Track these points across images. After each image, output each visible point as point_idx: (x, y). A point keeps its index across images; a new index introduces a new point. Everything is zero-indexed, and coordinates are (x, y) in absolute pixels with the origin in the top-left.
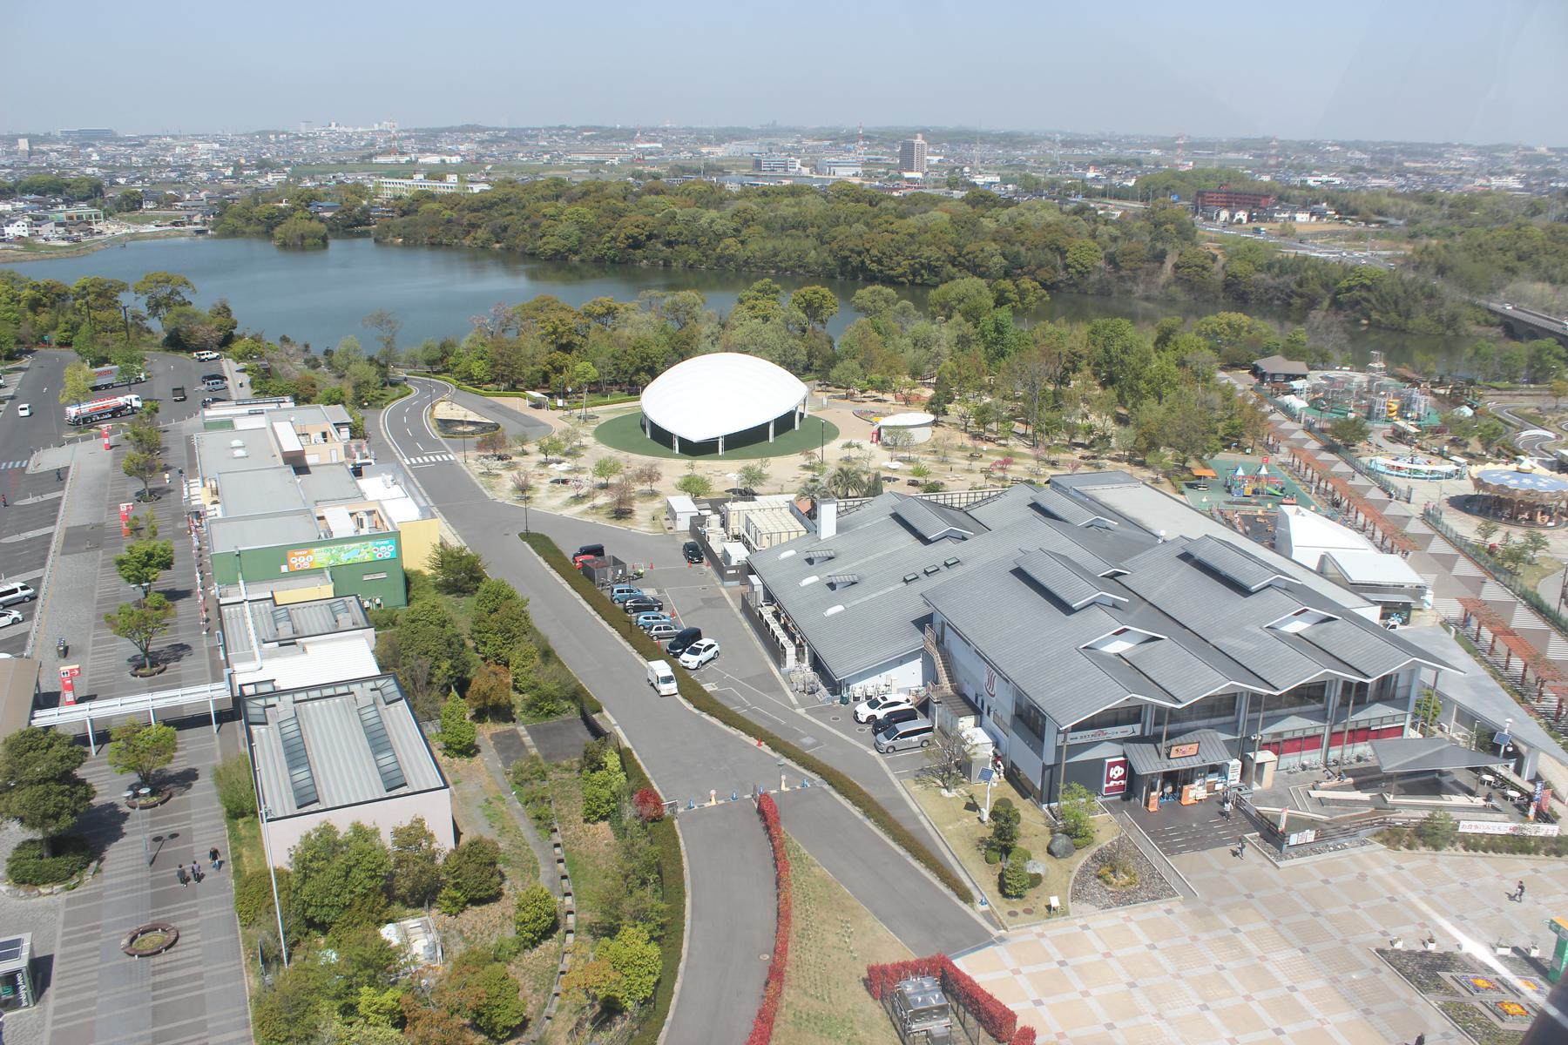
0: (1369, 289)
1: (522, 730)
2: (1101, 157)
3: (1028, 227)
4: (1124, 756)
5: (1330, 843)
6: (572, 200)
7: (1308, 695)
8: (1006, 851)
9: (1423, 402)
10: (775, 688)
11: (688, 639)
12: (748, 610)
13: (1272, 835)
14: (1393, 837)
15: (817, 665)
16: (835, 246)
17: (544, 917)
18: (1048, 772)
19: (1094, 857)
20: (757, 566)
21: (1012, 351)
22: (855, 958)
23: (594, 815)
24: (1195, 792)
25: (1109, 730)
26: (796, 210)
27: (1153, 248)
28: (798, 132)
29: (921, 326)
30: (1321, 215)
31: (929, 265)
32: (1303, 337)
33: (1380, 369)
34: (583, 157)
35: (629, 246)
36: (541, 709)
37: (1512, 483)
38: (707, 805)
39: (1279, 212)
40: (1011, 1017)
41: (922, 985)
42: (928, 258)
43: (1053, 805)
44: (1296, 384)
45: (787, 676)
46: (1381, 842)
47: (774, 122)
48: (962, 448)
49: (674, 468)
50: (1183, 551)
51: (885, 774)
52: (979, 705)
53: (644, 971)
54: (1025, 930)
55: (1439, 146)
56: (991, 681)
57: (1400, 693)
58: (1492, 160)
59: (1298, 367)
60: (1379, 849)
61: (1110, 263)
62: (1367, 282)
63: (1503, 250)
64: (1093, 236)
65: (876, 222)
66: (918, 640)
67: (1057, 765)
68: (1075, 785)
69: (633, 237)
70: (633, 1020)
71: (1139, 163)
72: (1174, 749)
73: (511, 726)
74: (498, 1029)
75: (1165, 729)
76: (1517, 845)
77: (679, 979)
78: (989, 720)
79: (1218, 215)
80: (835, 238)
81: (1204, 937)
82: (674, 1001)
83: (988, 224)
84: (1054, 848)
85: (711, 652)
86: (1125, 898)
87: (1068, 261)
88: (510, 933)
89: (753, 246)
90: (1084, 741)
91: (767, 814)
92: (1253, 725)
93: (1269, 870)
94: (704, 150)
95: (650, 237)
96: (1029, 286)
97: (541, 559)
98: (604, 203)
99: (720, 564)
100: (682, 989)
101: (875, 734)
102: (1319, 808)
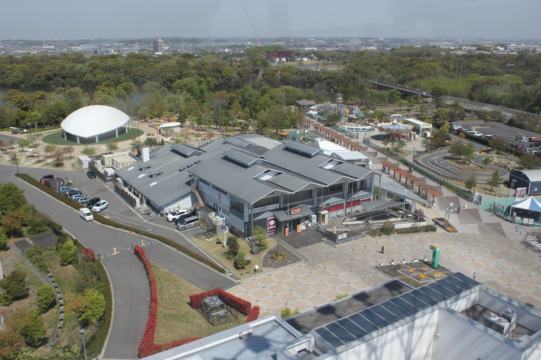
0: (332, 78)
1: (28, 239)
2: (229, 45)
3: (207, 64)
4: (274, 216)
5: (352, 238)
6: (18, 63)
7: (336, 189)
8: (235, 254)
9: (357, 109)
10: (134, 215)
11: (95, 202)
12: (118, 190)
13: (332, 237)
14: (373, 233)
15: (149, 203)
16: (132, 75)
17: (50, 297)
18: (246, 225)
19: (268, 253)
20: (119, 174)
21: (207, 100)
22: (183, 296)
23: (65, 263)
24: (301, 227)
25: (267, 207)
26: (115, 63)
27: (254, 69)
28: (111, 41)
29: (171, 96)
30: (312, 58)
31: (170, 80)
32: (312, 93)
33: (341, 100)
34: (20, 52)
35: (46, 79)
36: (35, 230)
37: (392, 128)
38: (113, 254)
39: (297, 58)
40: (249, 304)
41: (212, 299)
42: (169, 77)
43: (250, 238)
44: (312, 107)
45: (138, 210)
46: (370, 235)
47: (101, 37)
48: (193, 134)
49: (78, 148)
50: (285, 147)
51: (182, 237)
52: (216, 208)
53: (98, 306)
54: (247, 279)
55: (348, 38)
56: (220, 197)
57: (368, 186)
58: (366, 41)
59: (312, 102)
60: (369, 237)
61: (239, 75)
62: (332, 76)
63: (376, 65)
64: (231, 66)
65: (147, 65)
66: (188, 189)
67: (250, 222)
68: (257, 227)
69: (47, 76)
70: (96, 327)
71: (244, 46)
72: (292, 211)
73: (22, 238)
74: (36, 340)
75: (288, 205)
76: (414, 230)
77: (113, 311)
78: (221, 212)
79: (275, 60)
80: (132, 72)
81: (314, 272)
82: (112, 318)
83: (191, 63)
84: (253, 251)
85: (105, 205)
86: (284, 263)
87: (223, 75)
88: (35, 308)
89: (98, 76)
90: (259, 211)
91: (138, 253)
92: (319, 201)
93: (332, 248)
94: (72, 48)
95: (55, 75)
96: (211, 80)
97: (26, 182)
98: (33, 63)
99: (103, 177)
100: (115, 314)
101: (176, 225)
102: (346, 227)
